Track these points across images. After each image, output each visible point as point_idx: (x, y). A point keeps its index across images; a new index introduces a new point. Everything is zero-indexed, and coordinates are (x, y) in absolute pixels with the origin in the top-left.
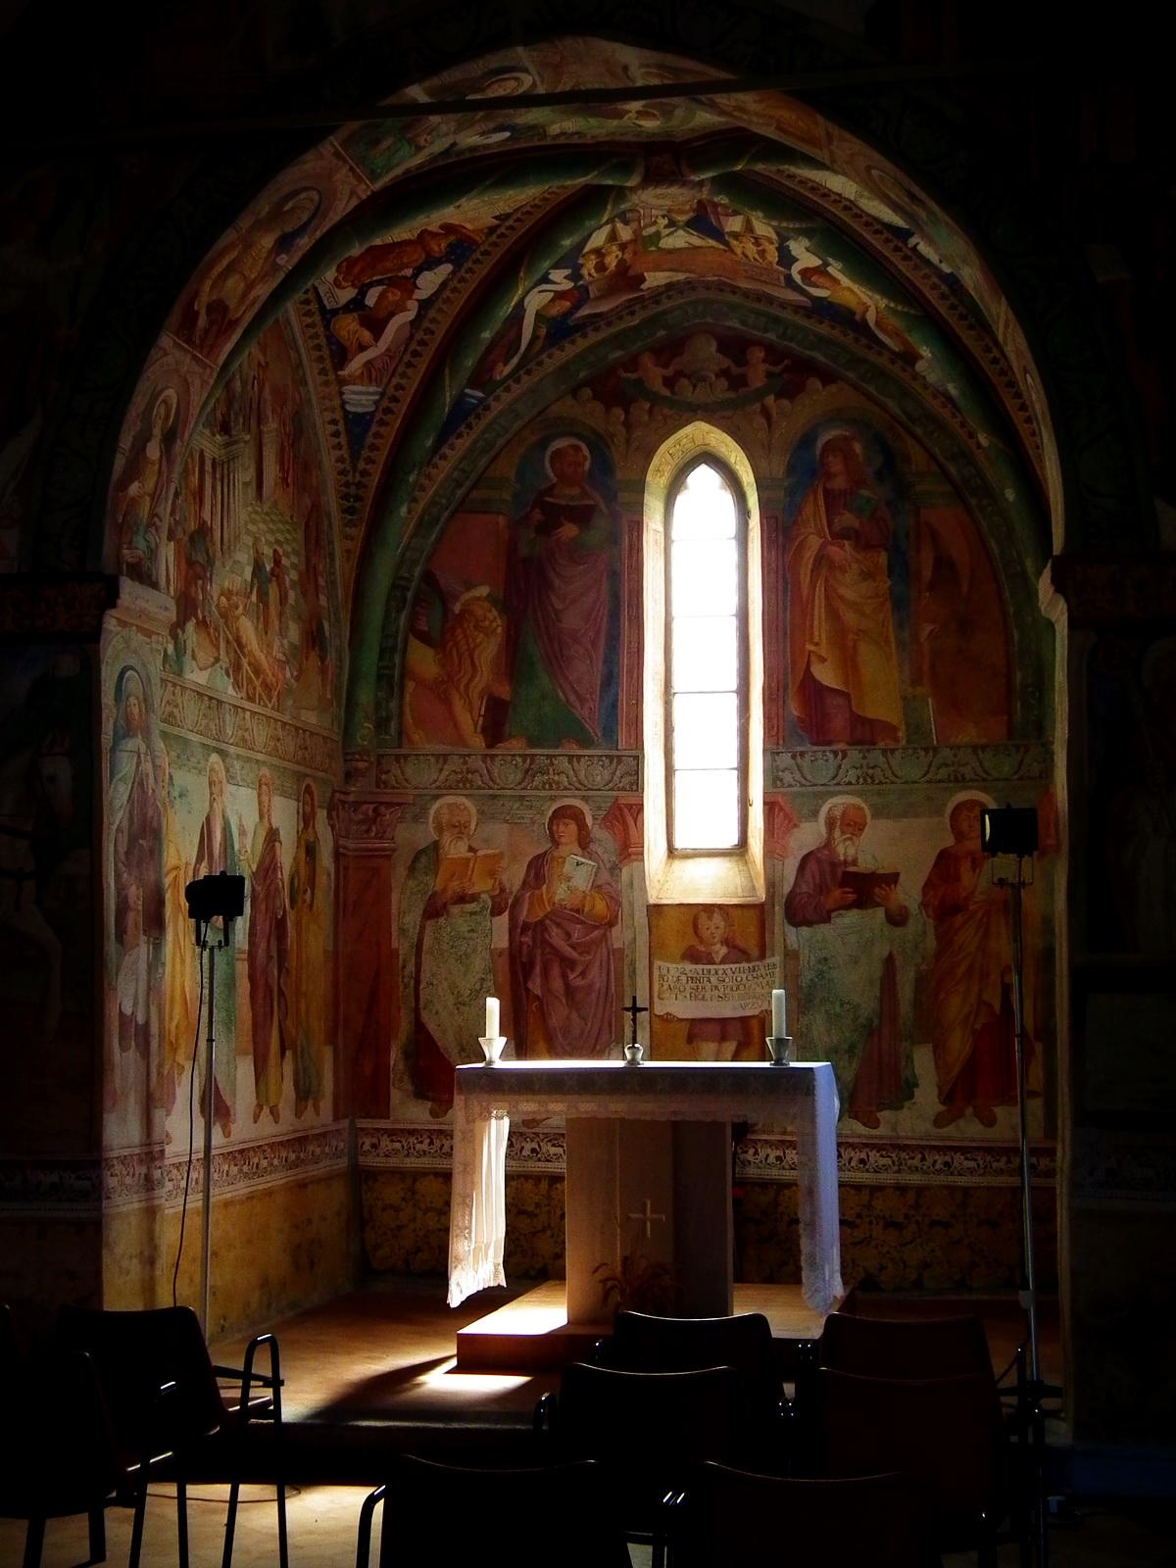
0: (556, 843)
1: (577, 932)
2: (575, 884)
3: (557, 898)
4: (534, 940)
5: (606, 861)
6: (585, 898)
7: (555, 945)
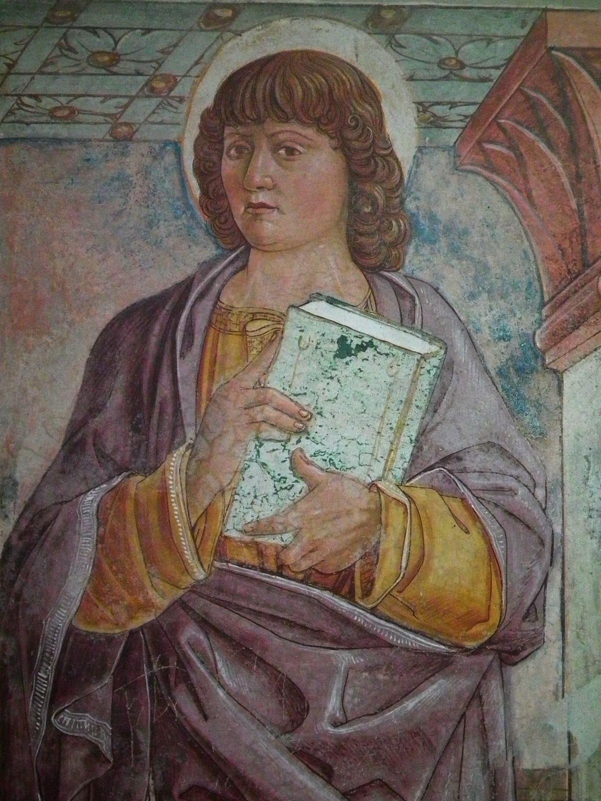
0: (235, 241)
1: (339, 690)
2: (330, 446)
3: (236, 522)
4: (123, 729)
5: (485, 335)
6: (377, 517)
7: (223, 747)
